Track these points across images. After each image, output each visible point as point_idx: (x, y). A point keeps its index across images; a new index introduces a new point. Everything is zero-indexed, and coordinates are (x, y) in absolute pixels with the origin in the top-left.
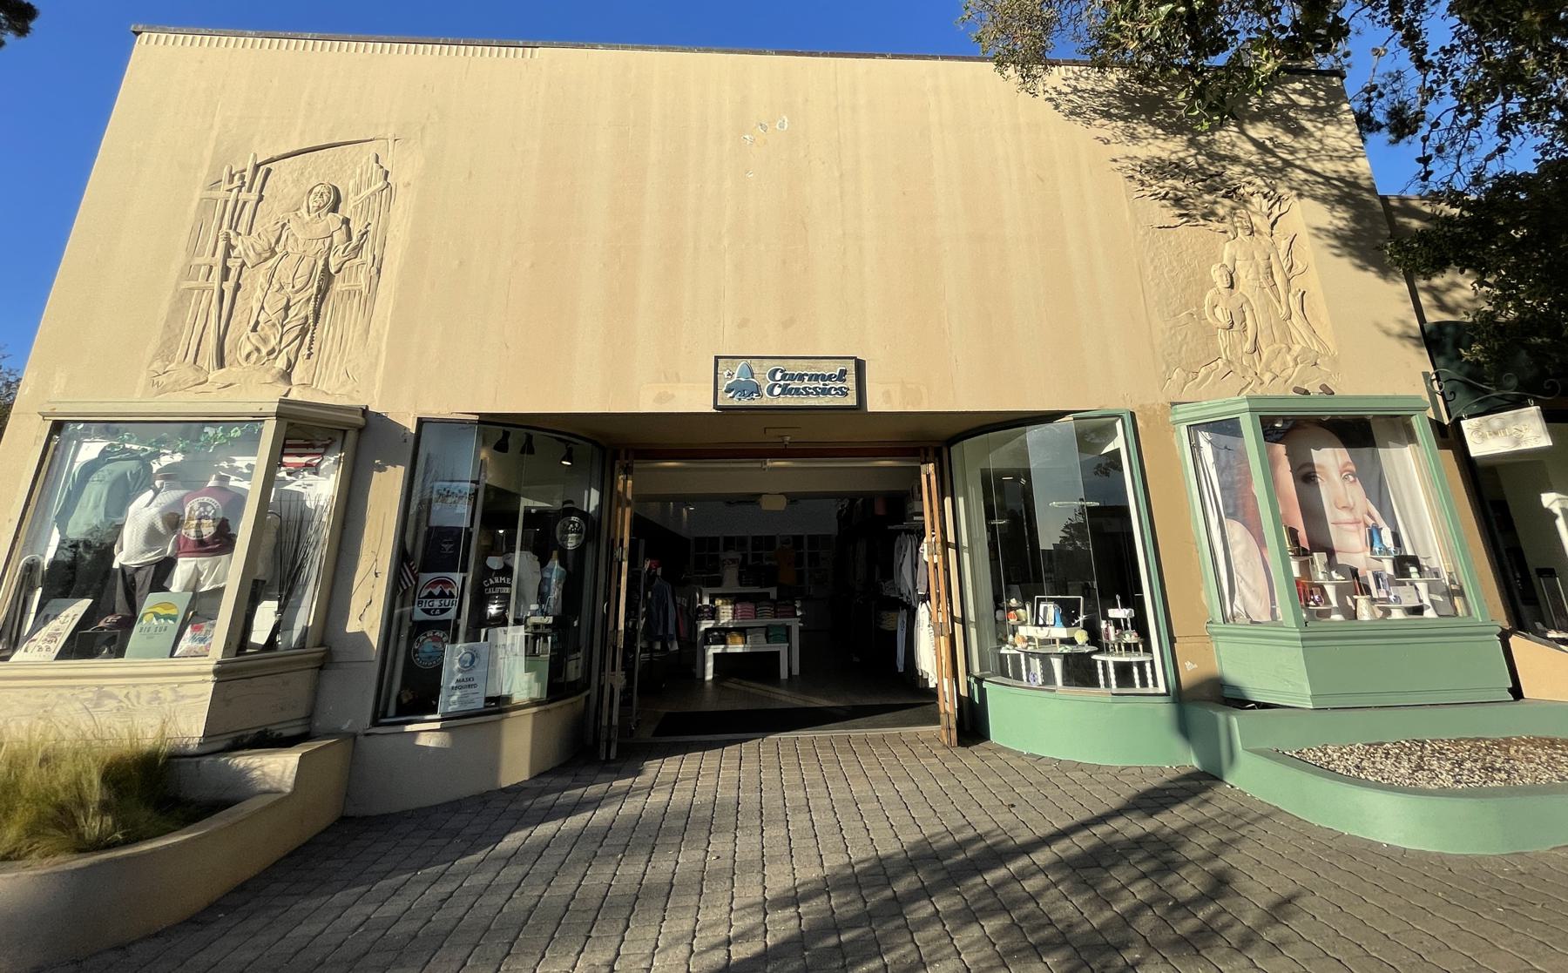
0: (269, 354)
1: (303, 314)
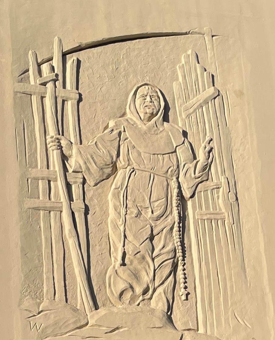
0: (145, 291)
1: (169, 247)
